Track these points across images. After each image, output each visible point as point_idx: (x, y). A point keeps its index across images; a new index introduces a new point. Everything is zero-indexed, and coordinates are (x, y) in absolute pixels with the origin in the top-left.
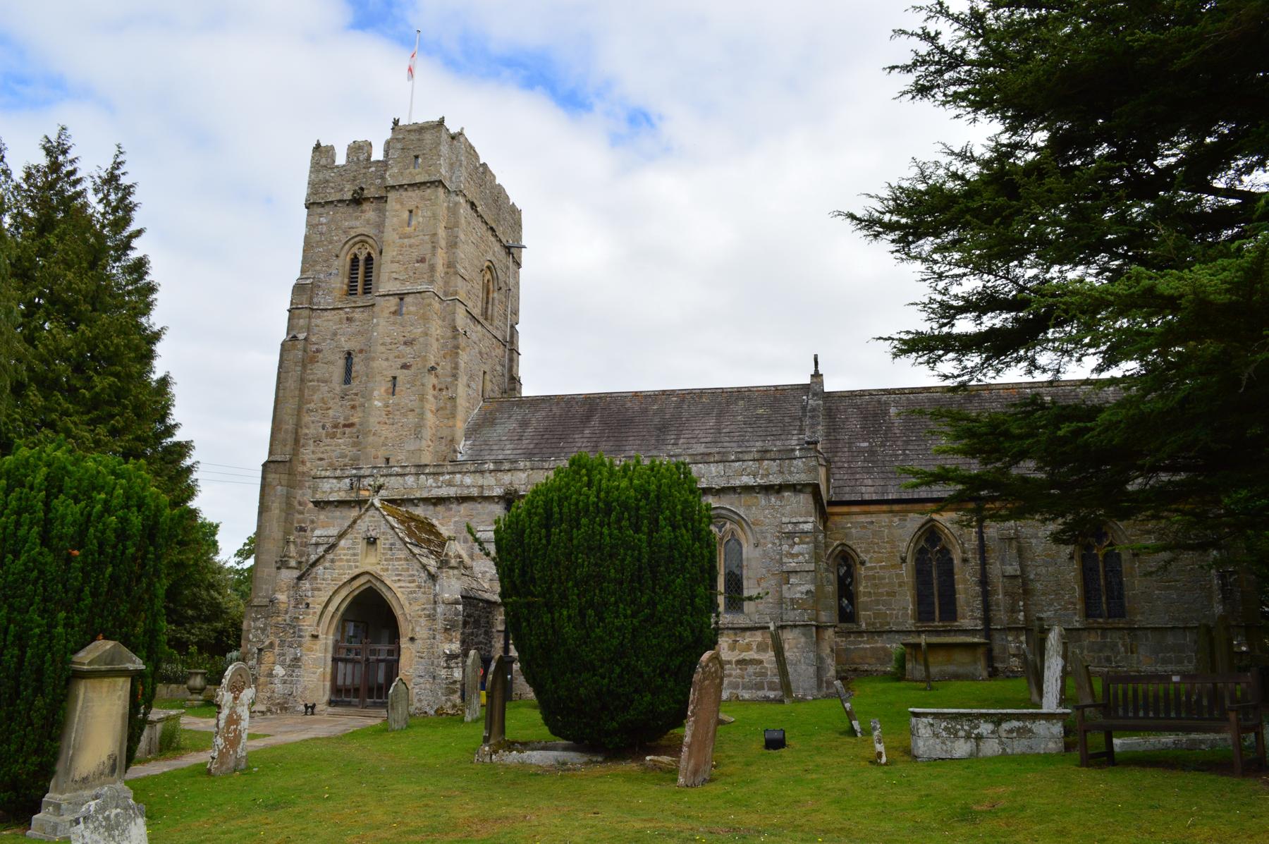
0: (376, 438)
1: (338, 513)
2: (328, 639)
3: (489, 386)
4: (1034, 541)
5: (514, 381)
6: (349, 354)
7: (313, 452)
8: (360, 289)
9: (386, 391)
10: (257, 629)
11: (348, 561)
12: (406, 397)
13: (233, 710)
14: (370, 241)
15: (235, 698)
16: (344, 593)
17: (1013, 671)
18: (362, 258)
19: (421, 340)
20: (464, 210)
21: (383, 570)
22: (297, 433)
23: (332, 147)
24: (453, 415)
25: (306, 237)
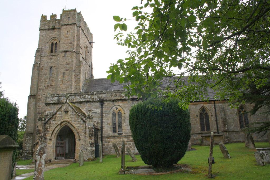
0: (60, 88)
1: (53, 107)
2: (54, 140)
3: (87, 76)
4: (228, 110)
5: (92, 75)
6: (51, 67)
7: (42, 93)
8: (54, 51)
9: (62, 76)
10: (28, 140)
11: (60, 118)
12: (67, 78)
13: (40, 161)
14: (56, 39)
15: (41, 158)
16: (59, 127)
17: (226, 142)
18: (54, 43)
19: (71, 63)
20: (81, 31)
21: (70, 120)
22: (37, 88)
23: (46, 16)
24: (79, 82)
25: (39, 38)
